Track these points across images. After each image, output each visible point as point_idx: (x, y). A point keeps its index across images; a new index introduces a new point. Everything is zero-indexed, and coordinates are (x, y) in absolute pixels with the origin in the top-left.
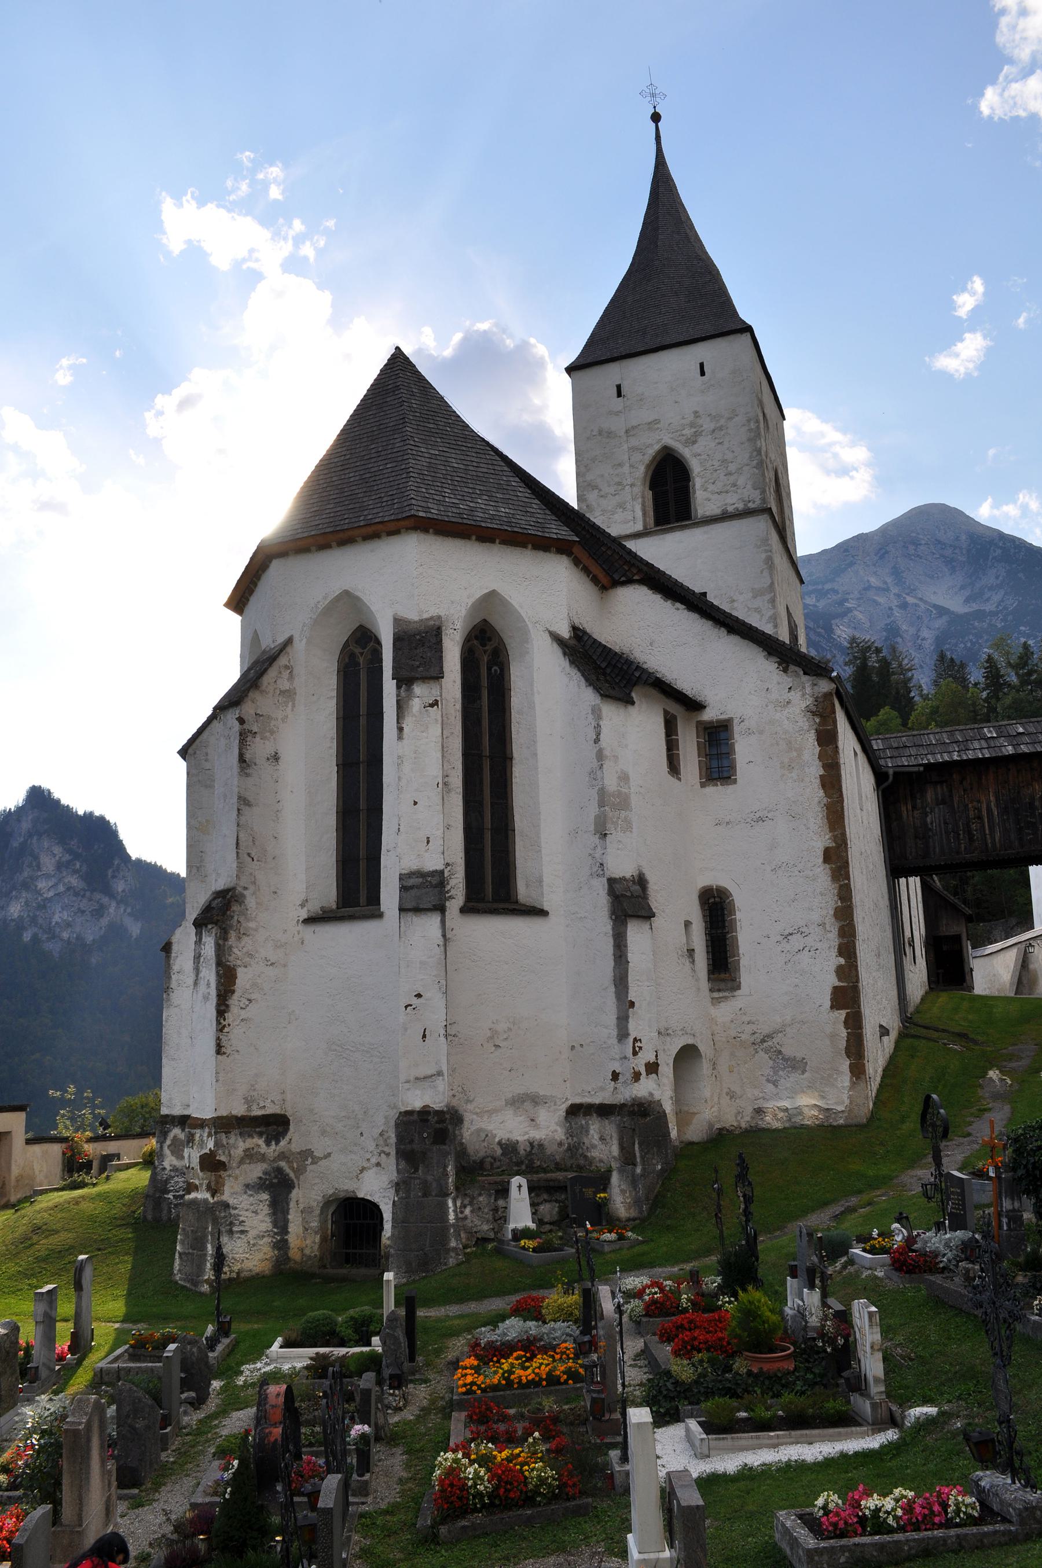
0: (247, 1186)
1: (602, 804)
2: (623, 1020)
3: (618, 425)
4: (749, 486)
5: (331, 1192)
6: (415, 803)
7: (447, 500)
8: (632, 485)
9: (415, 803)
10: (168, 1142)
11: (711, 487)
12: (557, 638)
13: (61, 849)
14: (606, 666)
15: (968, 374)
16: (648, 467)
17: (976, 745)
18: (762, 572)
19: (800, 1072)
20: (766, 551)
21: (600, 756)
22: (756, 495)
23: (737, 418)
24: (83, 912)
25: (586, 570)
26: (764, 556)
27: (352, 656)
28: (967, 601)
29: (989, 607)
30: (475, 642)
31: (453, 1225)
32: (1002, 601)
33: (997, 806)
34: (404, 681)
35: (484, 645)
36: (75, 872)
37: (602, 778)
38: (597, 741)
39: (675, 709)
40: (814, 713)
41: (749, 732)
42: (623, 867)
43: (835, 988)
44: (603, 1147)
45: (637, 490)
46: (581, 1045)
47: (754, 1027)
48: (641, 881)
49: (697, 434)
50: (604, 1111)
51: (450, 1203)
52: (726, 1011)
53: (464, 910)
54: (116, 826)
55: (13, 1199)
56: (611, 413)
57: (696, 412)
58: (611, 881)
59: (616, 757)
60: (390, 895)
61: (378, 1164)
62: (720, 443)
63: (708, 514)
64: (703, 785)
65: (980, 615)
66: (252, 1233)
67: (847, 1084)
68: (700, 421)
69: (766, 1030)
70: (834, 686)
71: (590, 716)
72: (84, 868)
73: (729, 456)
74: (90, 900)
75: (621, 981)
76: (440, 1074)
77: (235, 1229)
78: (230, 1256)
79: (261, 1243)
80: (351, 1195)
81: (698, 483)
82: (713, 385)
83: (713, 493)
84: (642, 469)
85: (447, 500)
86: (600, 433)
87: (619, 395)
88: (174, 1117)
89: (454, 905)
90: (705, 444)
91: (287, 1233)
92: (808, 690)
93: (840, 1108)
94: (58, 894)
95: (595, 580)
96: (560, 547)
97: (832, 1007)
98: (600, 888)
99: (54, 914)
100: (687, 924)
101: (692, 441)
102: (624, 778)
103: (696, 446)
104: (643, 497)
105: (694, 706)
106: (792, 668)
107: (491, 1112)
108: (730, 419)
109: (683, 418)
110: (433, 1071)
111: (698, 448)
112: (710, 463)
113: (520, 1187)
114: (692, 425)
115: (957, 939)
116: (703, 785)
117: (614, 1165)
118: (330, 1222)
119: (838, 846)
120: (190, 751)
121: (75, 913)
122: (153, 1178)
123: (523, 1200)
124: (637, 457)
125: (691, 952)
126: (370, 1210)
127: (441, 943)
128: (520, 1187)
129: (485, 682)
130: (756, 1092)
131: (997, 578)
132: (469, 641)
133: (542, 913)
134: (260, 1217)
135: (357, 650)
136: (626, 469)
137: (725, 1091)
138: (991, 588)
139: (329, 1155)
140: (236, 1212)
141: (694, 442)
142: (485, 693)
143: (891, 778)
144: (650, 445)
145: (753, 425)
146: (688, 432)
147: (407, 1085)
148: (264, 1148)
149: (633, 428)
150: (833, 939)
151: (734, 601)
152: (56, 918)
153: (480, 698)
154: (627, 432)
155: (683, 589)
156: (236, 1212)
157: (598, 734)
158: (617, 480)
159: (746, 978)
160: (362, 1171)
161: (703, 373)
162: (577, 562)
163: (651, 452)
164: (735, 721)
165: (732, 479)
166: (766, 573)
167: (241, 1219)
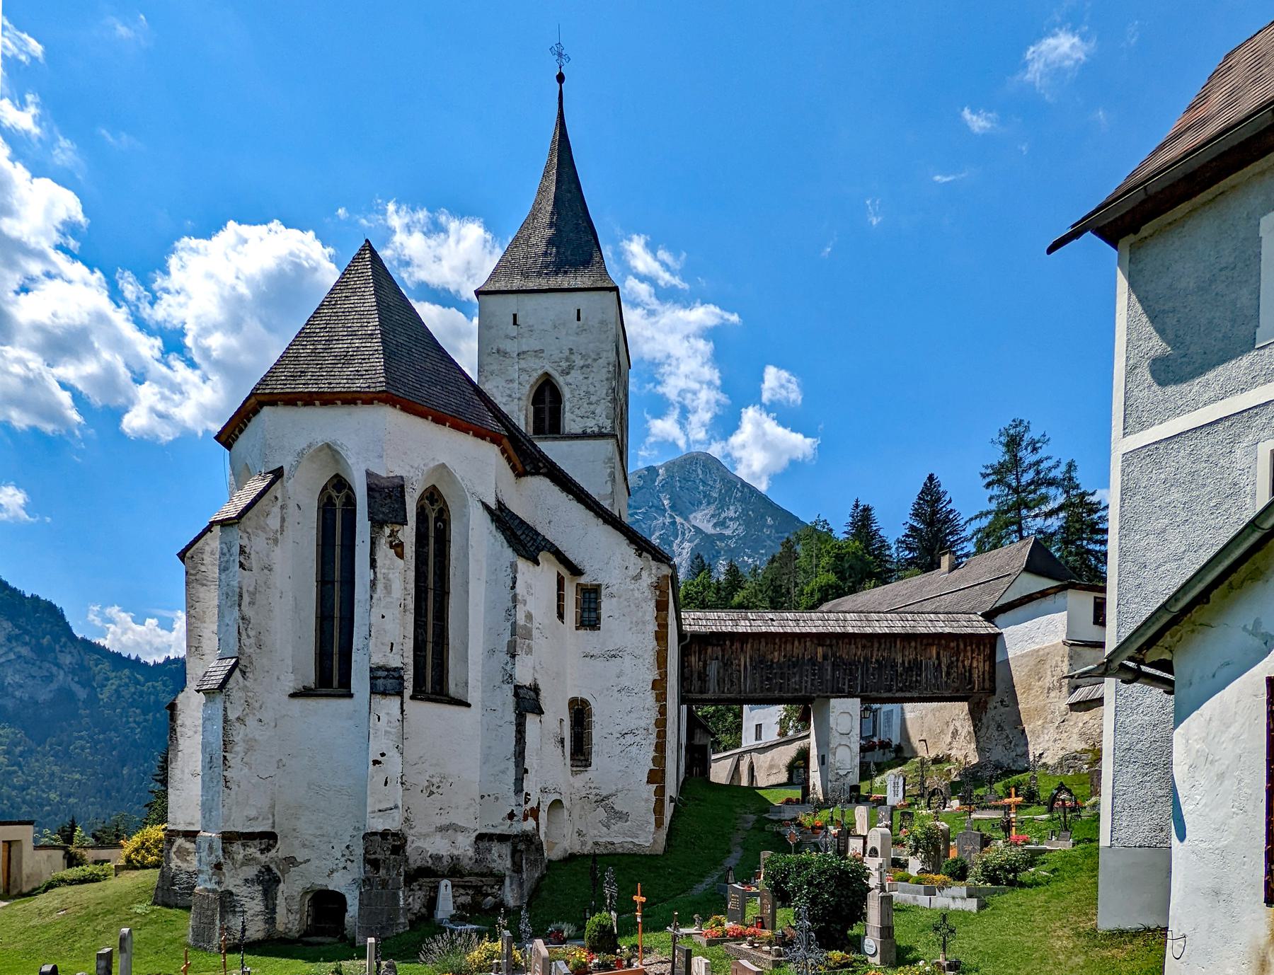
0: (246, 880)
1: (513, 633)
2: (519, 782)
3: (511, 347)
4: (604, 416)
5: (309, 886)
6: (383, 617)
7: (411, 383)
9: (383, 617)
10: (174, 849)
11: (577, 412)
12: (486, 507)
13: (10, 625)
14: (522, 535)
15: (14, 428)
17: (743, 623)
18: (606, 483)
19: (624, 821)
20: (611, 467)
21: (515, 599)
22: (608, 423)
23: (600, 361)
24: (34, 677)
25: (509, 459)
26: (609, 471)
27: (330, 498)
28: (715, 526)
29: (728, 532)
30: (426, 501)
31: (402, 908)
32: (736, 529)
33: (751, 665)
34: (377, 523)
35: (432, 504)
36: (26, 644)
37: (515, 615)
38: (513, 588)
39: (565, 573)
40: (656, 588)
41: (612, 596)
42: (524, 676)
43: (651, 770)
44: (500, 861)
45: (522, 403)
46: (489, 795)
47: (598, 791)
48: (535, 689)
49: (571, 368)
50: (502, 838)
51: (401, 894)
52: (579, 781)
53: (413, 698)
54: (62, 611)
55: (25, 890)
56: (507, 337)
57: (571, 349)
58: (517, 688)
59: (525, 601)
60: (360, 681)
61: (345, 868)
62: (586, 378)
63: (572, 431)
64: (577, 628)
65: (722, 537)
66: (250, 912)
67: (653, 830)
68: (573, 357)
69: (604, 794)
70: (671, 571)
71: (509, 570)
72: (33, 641)
73: (592, 389)
74: (40, 668)
75: (520, 754)
76: (396, 807)
77: (237, 909)
78: (234, 928)
79: (256, 919)
80: (324, 888)
81: (567, 405)
82: (585, 330)
83: (577, 416)
85: (411, 383)
86: (498, 351)
87: (515, 323)
88: (179, 831)
89: (408, 692)
90: (575, 376)
91: (275, 913)
92: (654, 571)
93: (648, 844)
94: (9, 661)
95: (514, 468)
96: (495, 440)
97: (648, 782)
98: (509, 690)
99: (6, 676)
100: (562, 720)
101: (566, 372)
102: (529, 617)
103: (569, 376)
104: (526, 410)
105: (576, 571)
106: (645, 554)
107: (426, 836)
108: (595, 360)
109: (561, 352)
110: (392, 805)
111: (569, 378)
112: (578, 392)
113: (446, 886)
114: (567, 359)
115: (705, 747)
116: (577, 628)
117: (507, 873)
118: (306, 906)
119: (662, 680)
120: (188, 554)
121: (26, 678)
122: (162, 875)
123: (449, 894)
124: (525, 377)
125: (562, 741)
126: (339, 899)
127: (400, 719)
128: (446, 886)
129: (432, 534)
130: (596, 832)
131: (735, 512)
132: (422, 500)
133: (469, 705)
134: (256, 902)
135: (334, 494)
136: (516, 385)
137: (576, 830)
138: (731, 519)
139: (309, 860)
140: (238, 898)
141: (568, 373)
142: (432, 541)
143: (689, 638)
144: (535, 370)
145: (611, 368)
146: (564, 364)
147: (373, 815)
148: (258, 855)
149: (524, 353)
150: (653, 739)
152: (9, 680)
153: (428, 545)
154: (518, 355)
155: (571, 483)
156: (238, 898)
157: (514, 583)
158: (508, 392)
159: (595, 759)
160: (332, 872)
161: (579, 319)
162: (503, 451)
163: (535, 375)
164: (603, 587)
165: (592, 407)
166: (609, 484)
167: (242, 903)
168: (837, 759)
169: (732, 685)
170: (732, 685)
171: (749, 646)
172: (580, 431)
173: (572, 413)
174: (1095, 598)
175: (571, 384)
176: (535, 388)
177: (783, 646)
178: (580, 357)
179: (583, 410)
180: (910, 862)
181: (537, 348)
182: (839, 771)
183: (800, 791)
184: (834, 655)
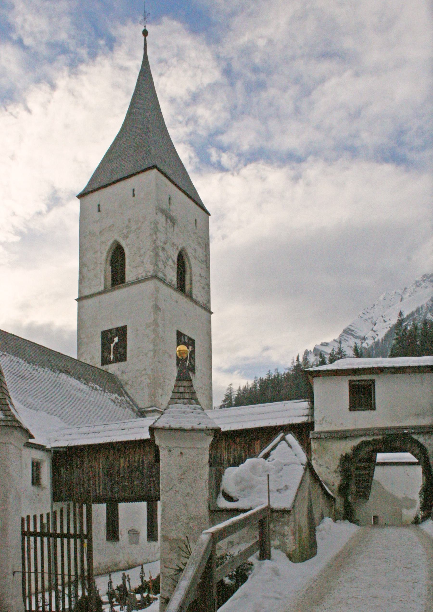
8: (101, 264)
15: (397, 322)
16: (108, 253)
26: (152, 303)
45: (103, 266)
49: (129, 232)
84: (105, 254)
101: (126, 237)
103: (128, 239)
111: (129, 241)
114: (127, 227)
141: (127, 237)
146: (125, 231)
151: (138, 330)
154: (100, 233)
161: (134, 195)
163: (109, 244)
171: (101, 455)
172: (134, 278)
174: (350, 381)
180: (100, 363)
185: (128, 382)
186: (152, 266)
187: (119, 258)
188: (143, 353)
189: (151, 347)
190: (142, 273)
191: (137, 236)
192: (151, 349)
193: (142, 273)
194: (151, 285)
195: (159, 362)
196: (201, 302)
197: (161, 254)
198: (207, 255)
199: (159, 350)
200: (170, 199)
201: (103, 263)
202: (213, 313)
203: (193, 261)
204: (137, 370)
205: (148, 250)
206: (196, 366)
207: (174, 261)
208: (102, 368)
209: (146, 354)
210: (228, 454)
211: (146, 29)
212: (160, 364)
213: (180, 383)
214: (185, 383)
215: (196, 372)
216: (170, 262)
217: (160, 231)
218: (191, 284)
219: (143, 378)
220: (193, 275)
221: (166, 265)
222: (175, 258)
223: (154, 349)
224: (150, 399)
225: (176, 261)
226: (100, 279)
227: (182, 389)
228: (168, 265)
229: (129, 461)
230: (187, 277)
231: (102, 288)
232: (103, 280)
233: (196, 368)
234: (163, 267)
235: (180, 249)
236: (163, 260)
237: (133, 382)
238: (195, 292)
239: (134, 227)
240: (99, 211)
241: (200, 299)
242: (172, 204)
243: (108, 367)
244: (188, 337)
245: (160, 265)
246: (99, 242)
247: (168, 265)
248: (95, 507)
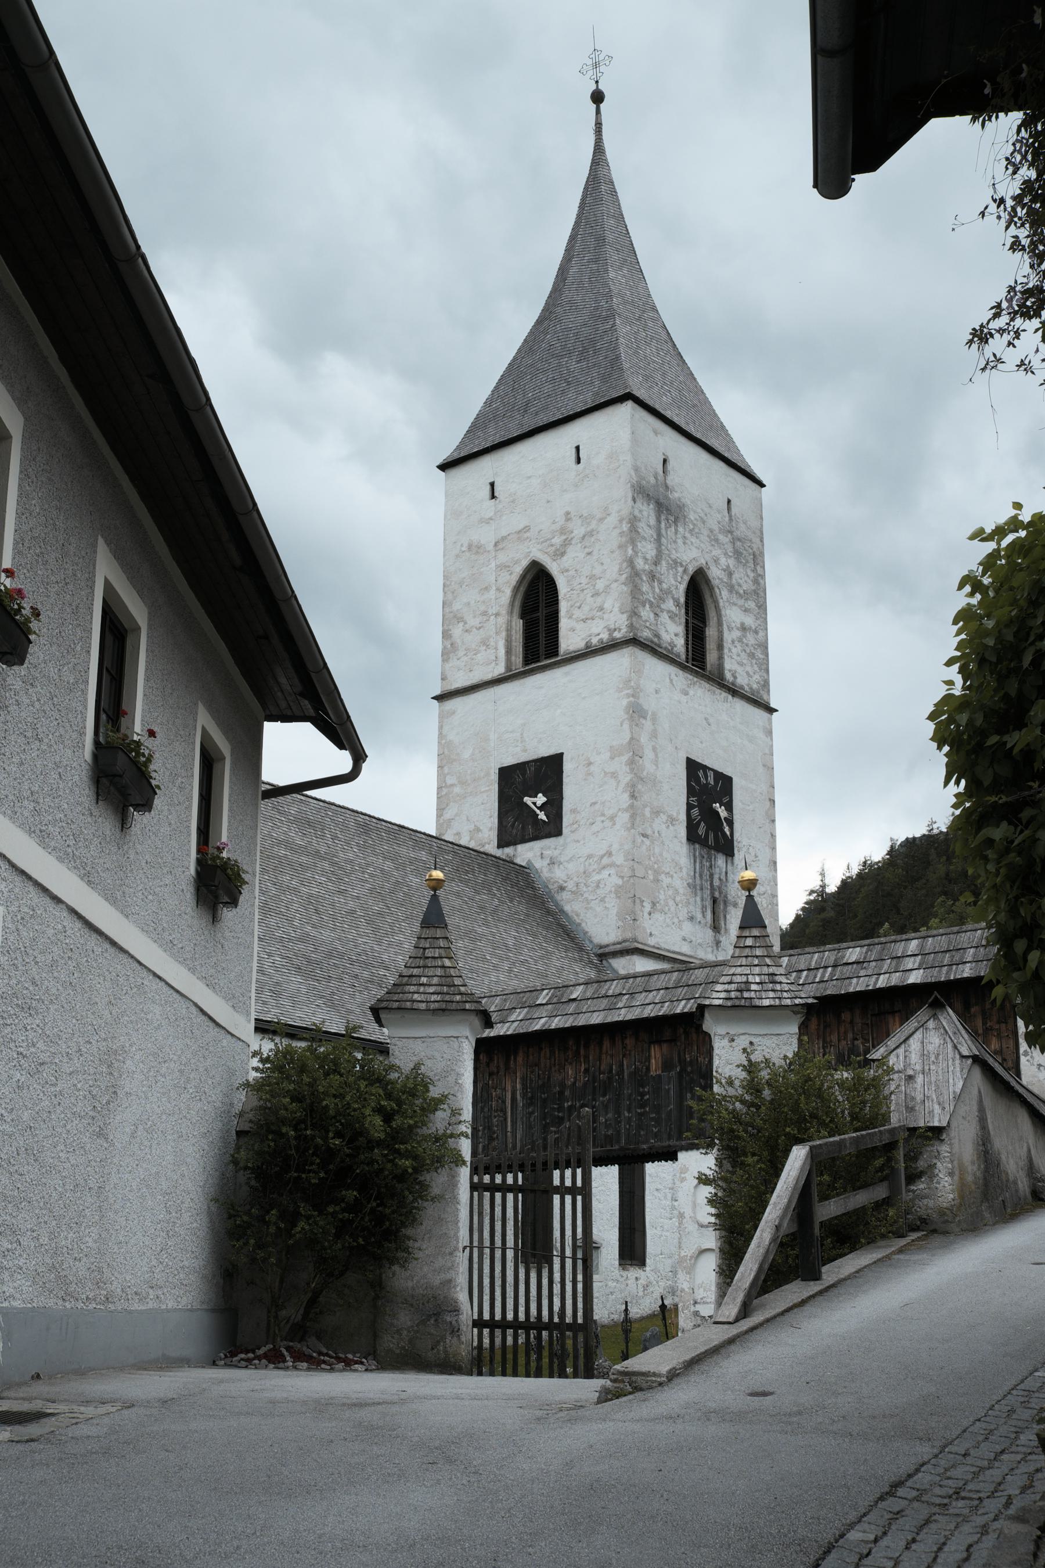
4: (616, 610)
8: (497, 615)
23: (609, 519)
26: (625, 702)
33: (524, 1095)
45: (502, 620)
49: (566, 543)
62: (589, 554)
68: (570, 525)
73: (597, 571)
84: (508, 592)
86: (470, 547)
90: (574, 554)
101: (560, 553)
103: (565, 558)
108: (601, 520)
114: (563, 531)
141: (563, 554)
146: (557, 540)
149: (504, 538)
151: (590, 764)
154: (496, 545)
161: (578, 461)
163: (519, 570)
165: (599, 600)
168: (698, 1281)
169: (491, 1139)
170: (491, 1139)
171: (520, 1059)
173: (570, 617)
175: (567, 571)
176: (522, 589)
177: (582, 1052)
178: (579, 522)
179: (586, 608)
181: (521, 526)
182: (698, 1307)
183: (496, 1330)
184: (682, 1062)
185: (565, 885)
186: (625, 616)
187: (542, 598)
188: (603, 815)
189: (625, 799)
190: (599, 634)
191: (587, 550)
192: (625, 805)
193: (599, 634)
194: (622, 661)
195: (645, 835)
196: (747, 688)
197: (645, 588)
198: (760, 578)
199: (645, 806)
200: (665, 461)
201: (504, 612)
202: (776, 711)
203: (724, 595)
204: (590, 856)
205: (616, 581)
206: (735, 839)
207: (676, 601)
208: (499, 853)
209: (612, 818)
210: (824, 1048)
211: (600, 87)
212: (645, 839)
213: (746, 933)
214: (756, 932)
215: (736, 851)
216: (670, 605)
217: (644, 538)
218: (720, 647)
219: (605, 873)
220: (725, 626)
221: (658, 611)
222: (681, 593)
223: (632, 806)
224: (620, 923)
225: (682, 600)
226: (496, 649)
227: (749, 942)
228: (662, 611)
229: (587, 1071)
230: (711, 632)
231: (500, 670)
232: (502, 652)
233: (735, 843)
234: (652, 616)
235: (691, 570)
236: (650, 601)
237: (577, 885)
238: (729, 665)
239: (579, 531)
240: (493, 496)
241: (742, 681)
242: (671, 472)
243: (516, 850)
244: (716, 772)
245: (646, 613)
246: (493, 565)
247: (662, 611)
248: (596, 1172)
